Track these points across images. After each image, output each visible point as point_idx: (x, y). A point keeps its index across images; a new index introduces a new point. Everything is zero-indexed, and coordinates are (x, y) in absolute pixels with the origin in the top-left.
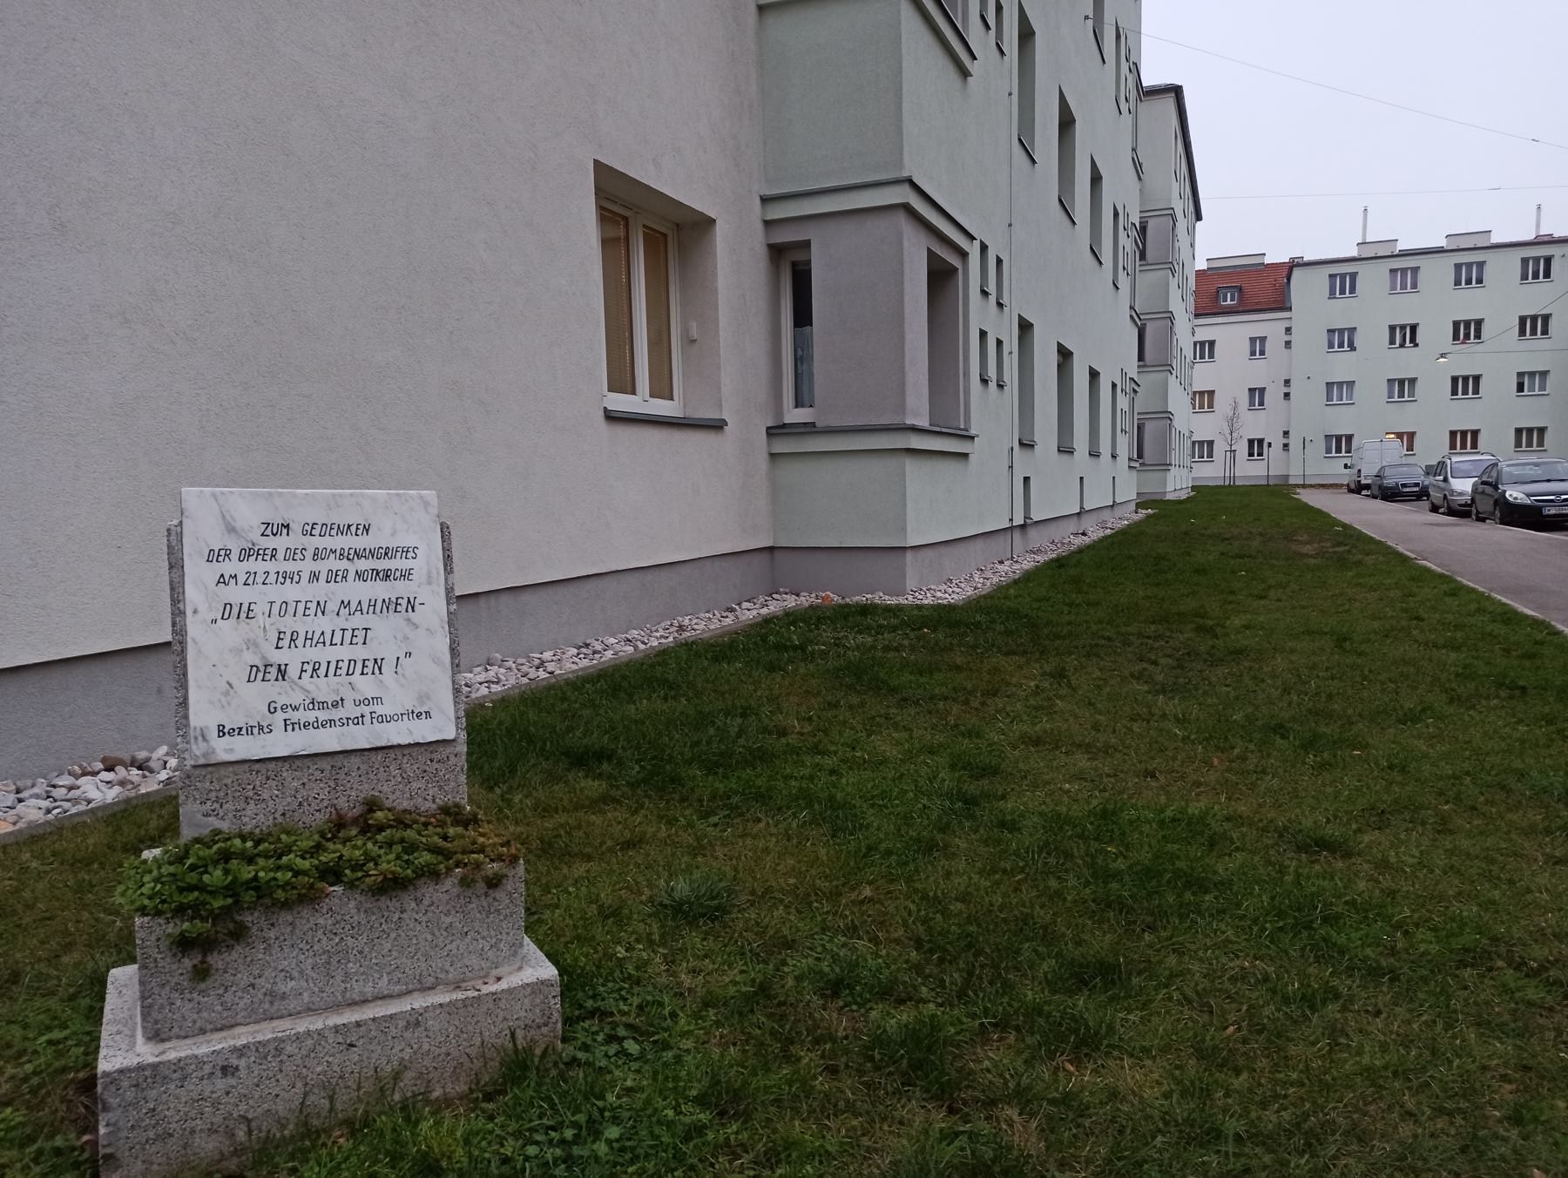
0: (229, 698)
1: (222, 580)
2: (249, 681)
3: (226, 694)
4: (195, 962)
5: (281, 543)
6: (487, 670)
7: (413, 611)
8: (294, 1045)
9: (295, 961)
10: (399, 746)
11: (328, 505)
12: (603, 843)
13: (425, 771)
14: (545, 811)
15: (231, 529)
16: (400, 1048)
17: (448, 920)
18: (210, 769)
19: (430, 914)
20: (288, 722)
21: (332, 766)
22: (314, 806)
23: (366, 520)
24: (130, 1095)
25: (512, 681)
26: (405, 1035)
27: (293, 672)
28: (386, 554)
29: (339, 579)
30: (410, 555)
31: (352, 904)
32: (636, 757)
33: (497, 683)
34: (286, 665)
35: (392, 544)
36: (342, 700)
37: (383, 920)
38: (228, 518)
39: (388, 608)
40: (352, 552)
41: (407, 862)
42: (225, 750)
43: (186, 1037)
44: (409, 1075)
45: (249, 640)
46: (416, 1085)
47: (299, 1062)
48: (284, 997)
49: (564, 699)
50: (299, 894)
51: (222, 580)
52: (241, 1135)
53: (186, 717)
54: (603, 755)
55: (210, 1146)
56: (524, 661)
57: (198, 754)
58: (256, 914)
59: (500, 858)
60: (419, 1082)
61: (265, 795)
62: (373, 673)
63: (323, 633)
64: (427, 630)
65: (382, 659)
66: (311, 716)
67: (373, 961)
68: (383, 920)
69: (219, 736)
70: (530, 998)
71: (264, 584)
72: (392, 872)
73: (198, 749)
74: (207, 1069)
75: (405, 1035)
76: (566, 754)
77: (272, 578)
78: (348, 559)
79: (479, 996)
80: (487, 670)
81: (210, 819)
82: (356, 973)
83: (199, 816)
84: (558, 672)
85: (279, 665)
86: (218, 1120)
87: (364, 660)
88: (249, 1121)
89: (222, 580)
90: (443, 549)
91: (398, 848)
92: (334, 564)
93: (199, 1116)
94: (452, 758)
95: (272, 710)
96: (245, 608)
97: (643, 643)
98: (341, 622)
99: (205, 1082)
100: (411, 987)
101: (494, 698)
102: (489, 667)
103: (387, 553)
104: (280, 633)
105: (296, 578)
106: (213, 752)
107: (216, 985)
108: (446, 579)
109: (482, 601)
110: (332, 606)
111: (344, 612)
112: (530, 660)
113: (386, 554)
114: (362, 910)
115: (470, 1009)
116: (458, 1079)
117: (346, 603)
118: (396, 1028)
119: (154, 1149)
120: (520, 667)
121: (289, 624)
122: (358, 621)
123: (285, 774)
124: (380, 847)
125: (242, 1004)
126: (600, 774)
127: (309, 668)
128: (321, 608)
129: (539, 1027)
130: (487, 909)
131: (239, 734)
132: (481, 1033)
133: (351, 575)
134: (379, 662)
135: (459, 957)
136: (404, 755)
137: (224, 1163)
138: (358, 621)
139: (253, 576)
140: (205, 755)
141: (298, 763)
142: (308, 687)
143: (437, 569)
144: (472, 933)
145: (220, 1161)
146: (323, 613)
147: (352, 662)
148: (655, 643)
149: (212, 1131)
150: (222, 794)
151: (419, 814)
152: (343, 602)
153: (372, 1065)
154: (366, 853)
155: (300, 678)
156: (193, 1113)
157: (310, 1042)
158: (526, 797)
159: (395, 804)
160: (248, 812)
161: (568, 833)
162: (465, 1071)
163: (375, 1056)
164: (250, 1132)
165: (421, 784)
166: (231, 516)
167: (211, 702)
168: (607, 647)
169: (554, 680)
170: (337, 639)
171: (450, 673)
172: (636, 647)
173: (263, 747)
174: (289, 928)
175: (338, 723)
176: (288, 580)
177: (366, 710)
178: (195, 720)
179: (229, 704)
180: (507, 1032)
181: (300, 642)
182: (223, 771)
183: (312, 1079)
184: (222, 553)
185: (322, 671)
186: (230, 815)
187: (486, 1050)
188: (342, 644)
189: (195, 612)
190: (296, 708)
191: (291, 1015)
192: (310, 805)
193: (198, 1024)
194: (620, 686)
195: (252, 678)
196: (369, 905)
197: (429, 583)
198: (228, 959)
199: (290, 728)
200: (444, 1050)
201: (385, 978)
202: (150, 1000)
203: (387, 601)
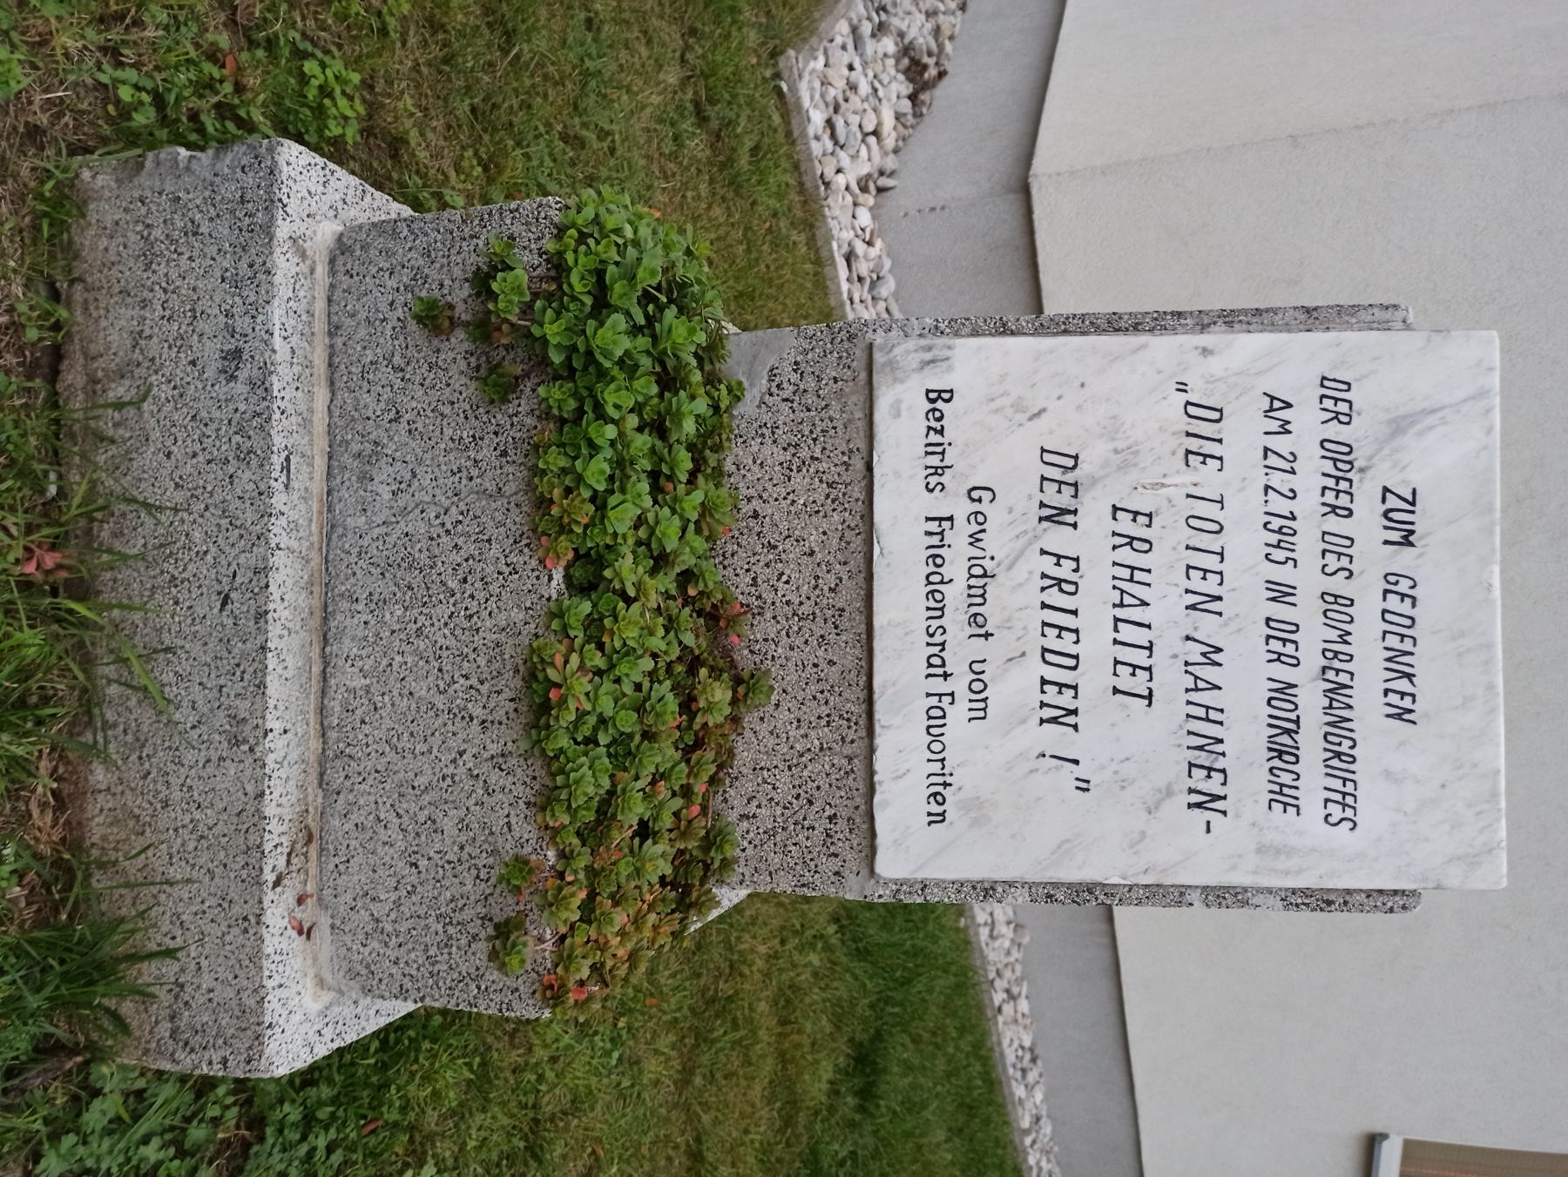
0: (1009, 412)
1: (1277, 404)
2: (1043, 450)
3: (1018, 407)
4: (460, 308)
5: (1366, 525)
6: (1009, 923)
7: (1190, 806)
8: (252, 486)
9: (428, 499)
10: (871, 750)
11: (1462, 634)
12: (706, 1106)
13: (810, 803)
14: (787, 1002)
15: (1399, 426)
16: (200, 703)
17: (448, 825)
18: (863, 375)
19: (468, 784)
20: (946, 525)
21: (843, 610)
22: (764, 574)
23: (1426, 715)
24: (229, 190)
25: (992, 956)
26: (221, 714)
27: (1057, 540)
28: (1338, 755)
29: (1276, 645)
30: (1336, 812)
31: (518, 616)
32: (859, 1152)
33: (991, 936)
34: (1075, 526)
35: (1363, 770)
36: (987, 635)
37: (474, 681)
38: (1429, 420)
39: (1201, 748)
40: (1343, 678)
41: (591, 741)
42: (899, 401)
43: (330, 301)
44: (146, 716)
45: (1136, 453)
46: (125, 731)
47: (218, 498)
48: (364, 478)
49: (962, 1030)
50: (551, 501)
51: (1276, 405)
52: (119, 391)
53: (975, 333)
54: (866, 1094)
55: (114, 337)
56: (1018, 973)
57: (896, 351)
58: (529, 421)
59: (564, 958)
60: (130, 738)
61: (798, 481)
62: (1043, 705)
63: (1144, 604)
64: (1143, 834)
65: (1075, 727)
66: (956, 568)
67: (398, 658)
68: (474, 681)
69: (928, 391)
70: (234, 1003)
71: (1267, 488)
72: (563, 701)
73: (906, 351)
74: (242, 324)
75: (221, 714)
76: (878, 1036)
77: (1282, 506)
78: (1324, 669)
79: (260, 884)
80: (1009, 923)
81: (764, 381)
82: (382, 622)
83: (772, 362)
84: (1000, 1019)
85: (1075, 512)
86: (154, 348)
87: (1075, 688)
88: (137, 404)
89: (1276, 405)
90: (1348, 892)
91: (628, 722)
92: (1313, 636)
93: (167, 313)
94: (834, 864)
95: (975, 495)
96: (1210, 448)
97: (1034, 1142)
98: (1169, 645)
99: (221, 319)
100: (333, 735)
101: (971, 932)
102: (1012, 926)
103: (1340, 758)
104: (1150, 516)
105: (1279, 555)
106: (895, 380)
107: (411, 352)
108: (1270, 891)
109: (1104, 927)
110: (1207, 627)
111: (1194, 652)
112: (1019, 981)
113: (1338, 755)
114: (502, 637)
115: (241, 860)
116: (115, 822)
117: (1215, 657)
118: (237, 695)
119: (133, 238)
120: (1010, 967)
121: (1170, 537)
122: (1170, 680)
123: (836, 517)
124: (638, 687)
125: (367, 399)
126: (837, 1093)
127: (1065, 571)
128: (1202, 605)
129: (172, 1018)
130: (457, 917)
131: (929, 428)
132: (189, 881)
133: (1284, 673)
134: (1071, 720)
135: (370, 846)
136: (850, 759)
137: (82, 361)
138: (1170, 680)
139: (1287, 466)
140: (892, 365)
141: (857, 543)
142: (1020, 572)
143: (1299, 872)
144: (414, 879)
145: (85, 354)
146: (1193, 607)
147: (1072, 662)
148: (1032, 1161)
149: (138, 337)
150: (810, 399)
151: (713, 780)
152: (1219, 650)
153: (180, 642)
154: (627, 651)
155: (1043, 552)
156: (174, 301)
157: (250, 516)
158: (815, 974)
159: (748, 734)
160: (767, 450)
161: (736, 1043)
162: (128, 839)
163: (196, 649)
164: (119, 406)
165: (784, 792)
166: (1431, 428)
167: (1003, 378)
168: (1030, 1088)
169: (989, 1013)
170: (1127, 633)
171: (1030, 878)
172: (1027, 1132)
173: (897, 474)
174: (490, 486)
175: (935, 623)
176: (1274, 538)
177: (959, 684)
178: (966, 349)
179: (997, 411)
180: (179, 942)
181: (1126, 556)
182: (856, 400)
183: (182, 521)
184: (1343, 407)
185: (1054, 597)
186: (765, 418)
187: (154, 890)
188: (1116, 642)
189: (1206, 352)
190: (975, 540)
191: (329, 493)
192: (767, 565)
193: (348, 322)
194: (974, 1116)
195: (1048, 457)
196: (509, 651)
197: (1261, 850)
198: (453, 370)
199: (933, 527)
200: (177, 795)
201: (360, 682)
202: (405, 232)
203: (1219, 748)
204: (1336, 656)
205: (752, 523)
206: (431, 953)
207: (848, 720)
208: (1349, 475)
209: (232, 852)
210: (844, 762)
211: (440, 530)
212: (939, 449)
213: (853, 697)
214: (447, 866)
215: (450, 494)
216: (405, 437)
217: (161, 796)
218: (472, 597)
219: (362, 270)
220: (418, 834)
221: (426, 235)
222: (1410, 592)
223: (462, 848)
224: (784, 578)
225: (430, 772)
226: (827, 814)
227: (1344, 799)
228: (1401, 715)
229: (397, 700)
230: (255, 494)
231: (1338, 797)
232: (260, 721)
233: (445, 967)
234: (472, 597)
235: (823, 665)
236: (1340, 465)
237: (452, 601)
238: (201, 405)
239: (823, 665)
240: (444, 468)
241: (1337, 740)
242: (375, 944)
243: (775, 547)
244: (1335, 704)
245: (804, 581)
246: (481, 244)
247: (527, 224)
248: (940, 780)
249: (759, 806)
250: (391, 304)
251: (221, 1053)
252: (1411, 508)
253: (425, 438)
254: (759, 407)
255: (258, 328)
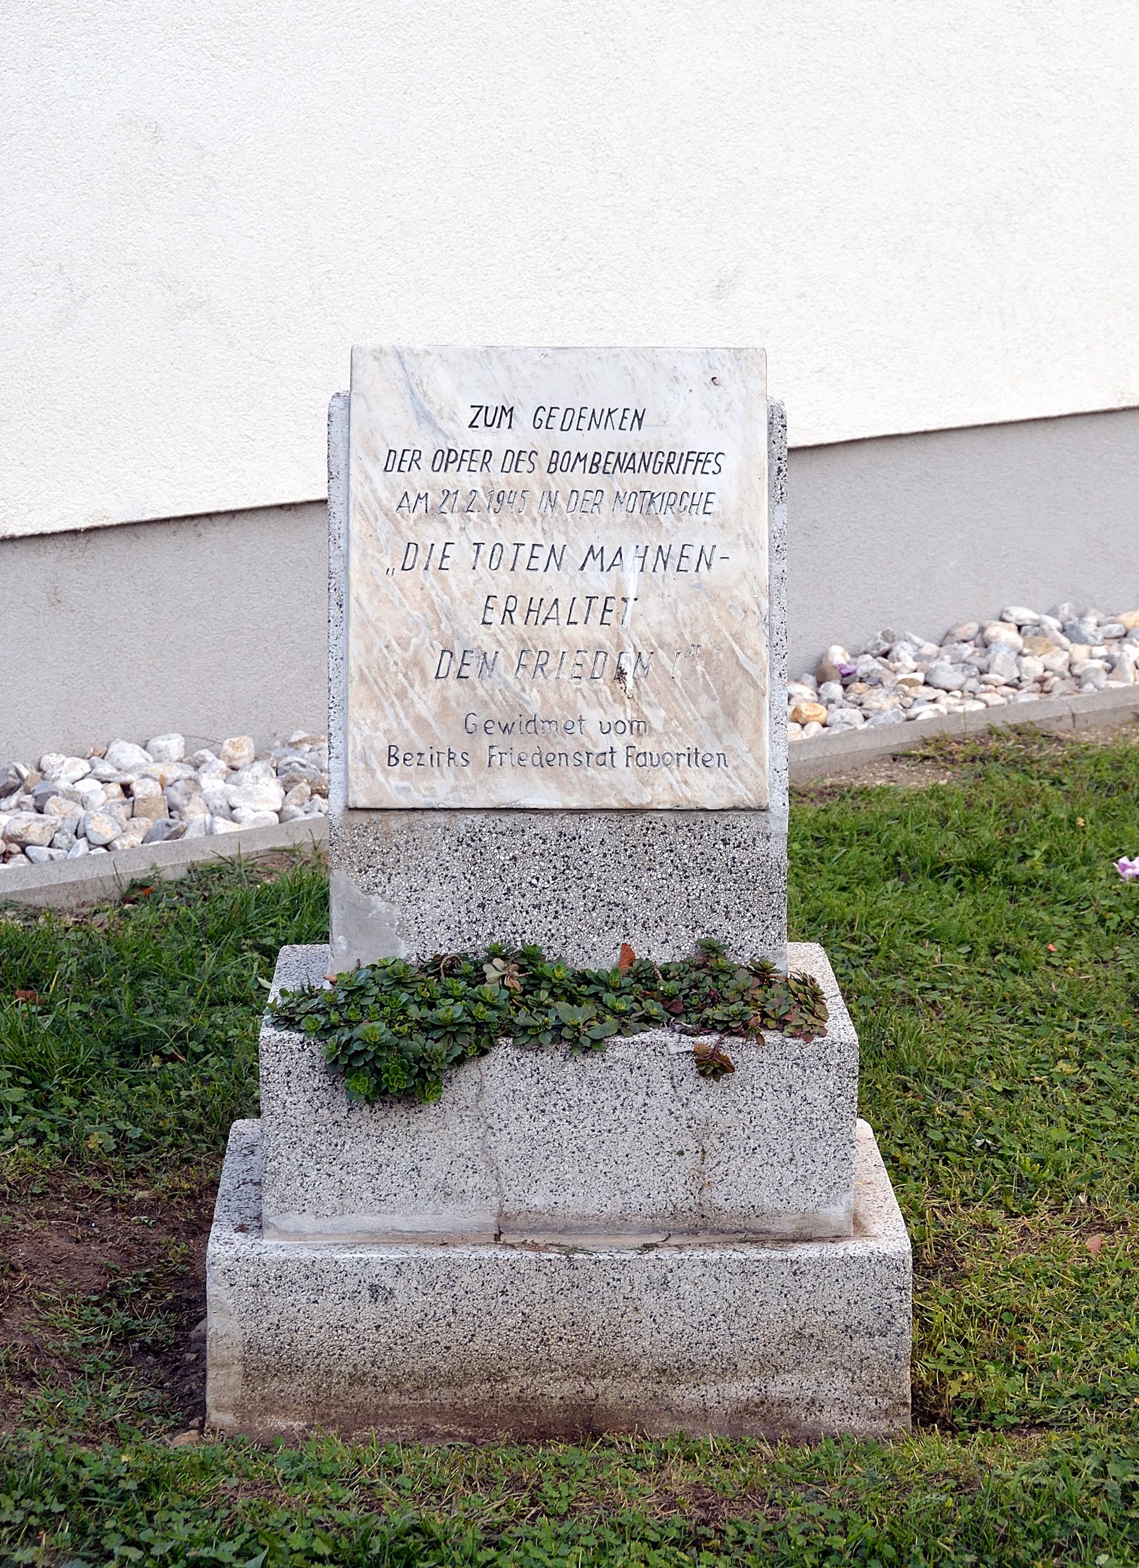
5: (498, 440)
15: (425, 417)
40: (612, 459)
67: (600, 1166)
68: (618, 1103)
74: (351, 1284)
99: (346, 1303)
103: (671, 462)
110: (574, 556)
130: (790, 1114)
184: (408, 456)
192: (524, 896)
200: (706, 1336)
202: (275, 1163)
204: (596, 464)
205: (488, 909)
206: (817, 1136)
207: (648, 829)
208: (460, 453)
209: (747, 1287)
210: (680, 832)
211: (505, 1132)
212: (436, 756)
213: (630, 826)
214: (754, 1123)
215: (477, 1125)
216: (432, 1163)
217: (707, 1350)
218: (555, 1105)
219: (300, 1201)
220: (731, 1148)
221: (279, 1145)
222: (548, 410)
223: (740, 1111)
224: (534, 881)
225: (685, 1139)
226: (722, 847)
227: (700, 459)
228: (639, 418)
229: (632, 1167)
230: (480, 1271)
231: (700, 465)
232: (650, 1264)
233: (827, 1123)
234: (555, 1105)
235: (604, 850)
236: (451, 459)
237: (558, 1122)
238: (410, 1320)
239: (604, 850)
240: (458, 1130)
241: (658, 465)
242: (814, 1182)
243: (509, 889)
244: (631, 466)
245: (535, 866)
246: (291, 1099)
247: (279, 1061)
248: (693, 759)
249: (718, 903)
250: (329, 1175)
251: (894, 1292)
252: (484, 409)
253: (434, 1146)
254: (393, 902)
255: (355, 1271)
